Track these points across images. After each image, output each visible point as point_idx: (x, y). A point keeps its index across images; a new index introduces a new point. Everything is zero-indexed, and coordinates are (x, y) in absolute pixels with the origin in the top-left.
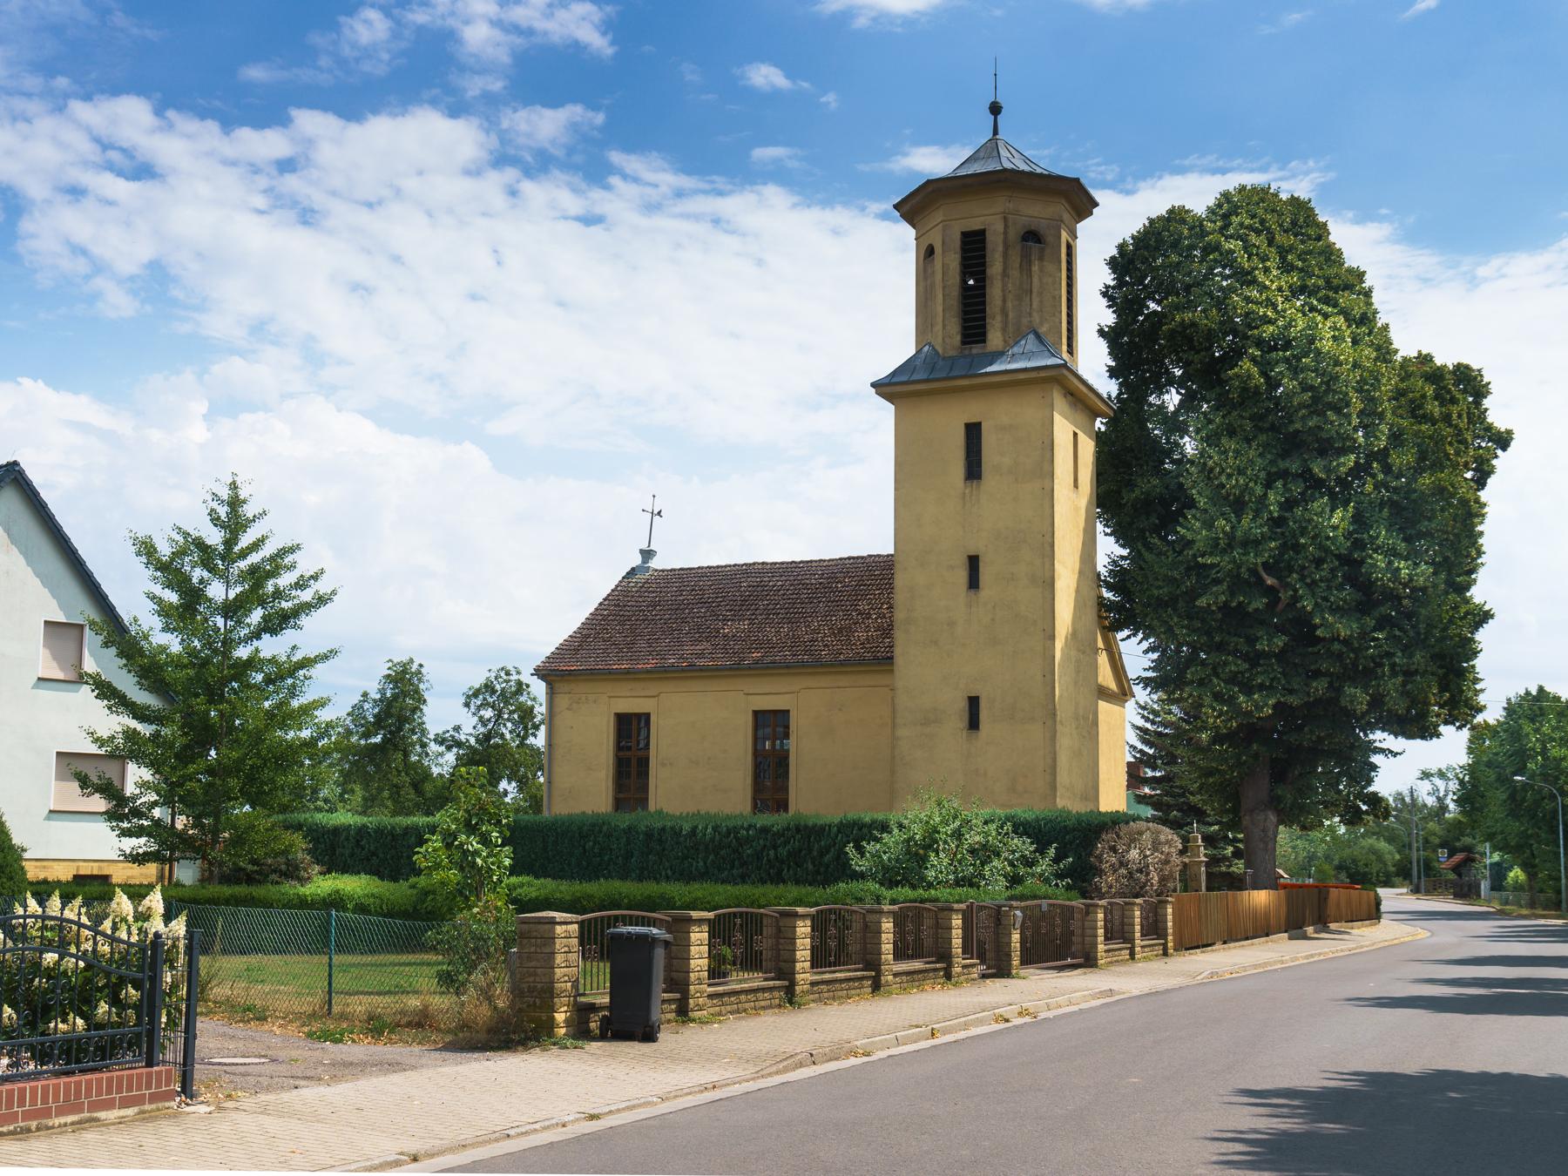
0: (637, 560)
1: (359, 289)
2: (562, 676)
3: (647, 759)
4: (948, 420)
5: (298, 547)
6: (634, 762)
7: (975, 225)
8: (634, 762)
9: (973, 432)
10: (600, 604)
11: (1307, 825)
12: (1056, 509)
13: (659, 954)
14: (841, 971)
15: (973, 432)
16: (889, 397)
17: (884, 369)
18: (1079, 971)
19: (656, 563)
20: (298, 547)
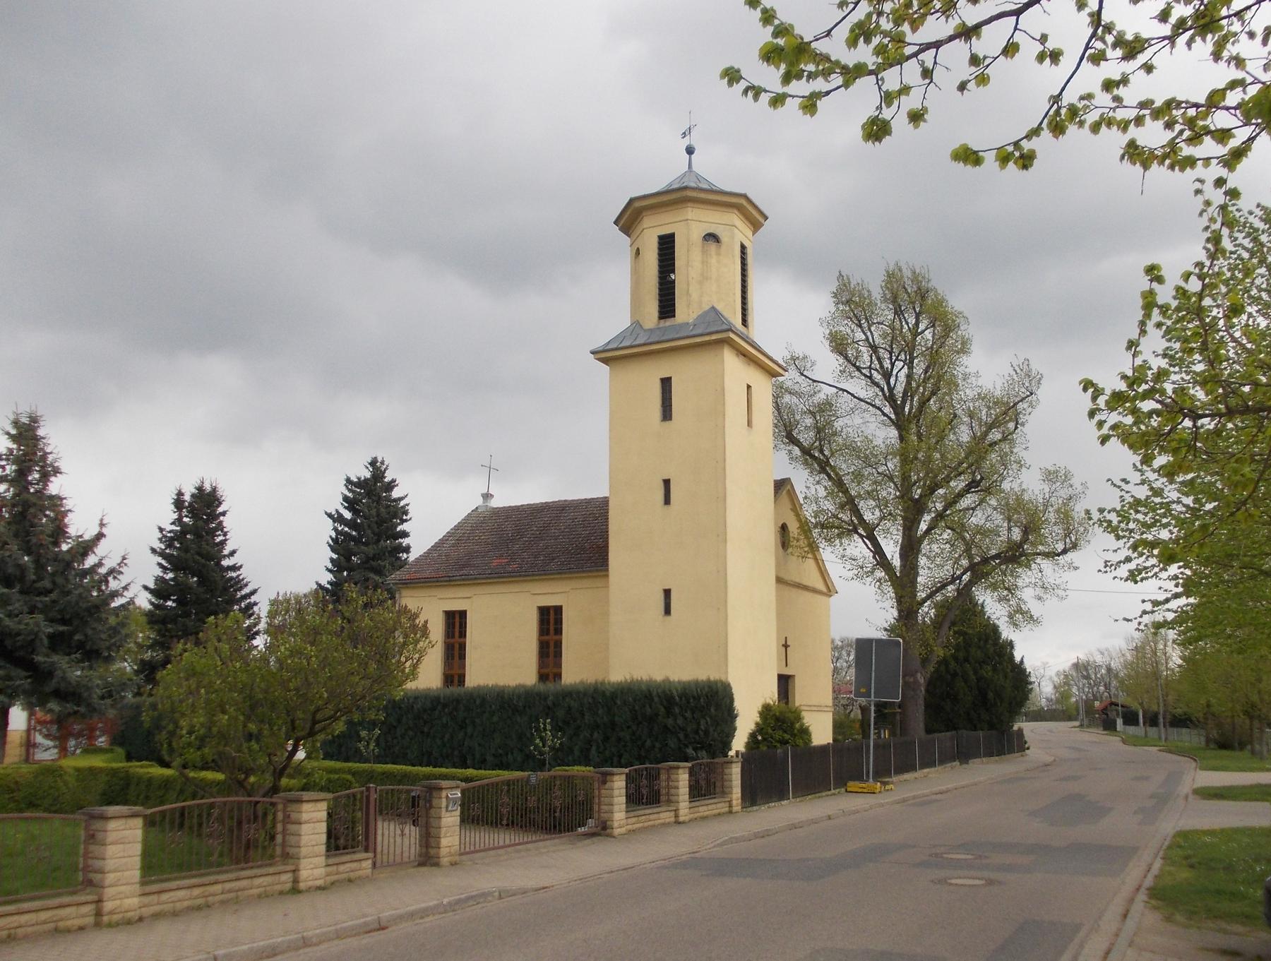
0: (479, 501)
1: (1040, 598)
2: (406, 584)
3: (465, 644)
4: (646, 378)
5: (326, 513)
6: (552, 645)
7: (666, 231)
8: (552, 645)
9: (666, 383)
10: (448, 533)
11: (190, 696)
12: (727, 440)
13: (898, 717)
14: (184, 878)
15: (666, 383)
16: (605, 361)
17: (599, 343)
18: (595, 839)
19: (496, 503)
20: (326, 513)
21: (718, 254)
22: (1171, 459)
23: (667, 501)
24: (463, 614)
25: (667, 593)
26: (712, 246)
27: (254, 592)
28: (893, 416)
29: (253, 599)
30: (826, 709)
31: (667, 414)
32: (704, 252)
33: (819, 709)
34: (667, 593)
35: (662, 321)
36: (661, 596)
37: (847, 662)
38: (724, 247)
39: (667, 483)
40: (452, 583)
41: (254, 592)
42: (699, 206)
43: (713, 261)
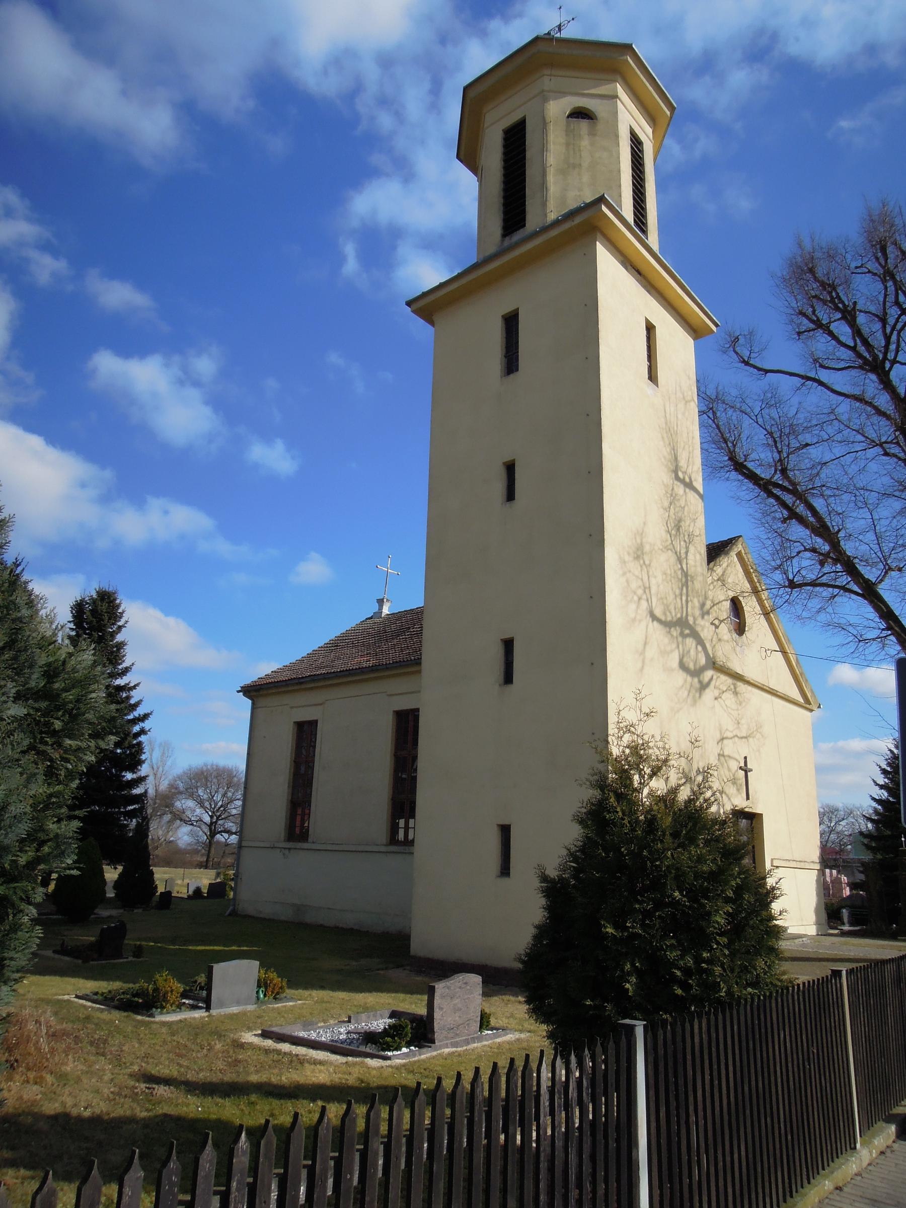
15: (511, 322)
21: (592, 133)
22: (358, 1129)
23: (510, 495)
24: (313, 724)
25: (508, 645)
26: (584, 124)
27: (145, 717)
28: (902, 455)
29: (146, 725)
30: (375, 849)
31: (511, 364)
32: (568, 132)
33: (802, 865)
34: (508, 645)
35: (507, 238)
36: (498, 652)
37: (829, 827)
38: (600, 126)
39: (510, 468)
40: (303, 686)
41: (145, 717)
42: (607, 243)
43: (585, 143)
